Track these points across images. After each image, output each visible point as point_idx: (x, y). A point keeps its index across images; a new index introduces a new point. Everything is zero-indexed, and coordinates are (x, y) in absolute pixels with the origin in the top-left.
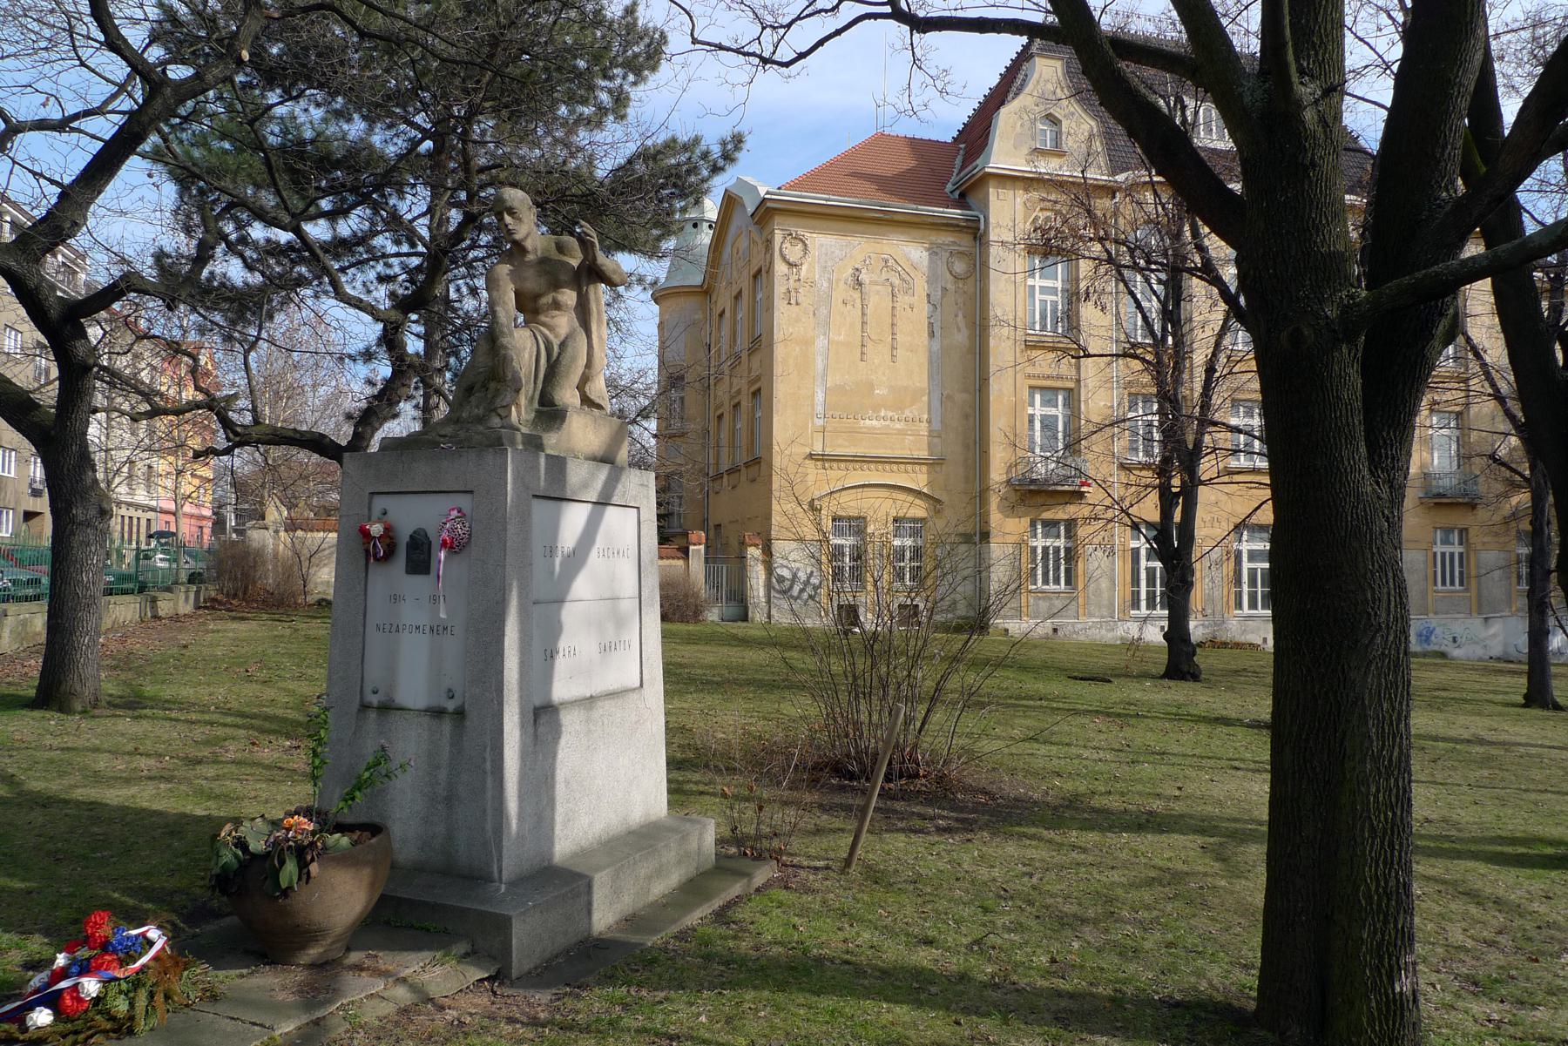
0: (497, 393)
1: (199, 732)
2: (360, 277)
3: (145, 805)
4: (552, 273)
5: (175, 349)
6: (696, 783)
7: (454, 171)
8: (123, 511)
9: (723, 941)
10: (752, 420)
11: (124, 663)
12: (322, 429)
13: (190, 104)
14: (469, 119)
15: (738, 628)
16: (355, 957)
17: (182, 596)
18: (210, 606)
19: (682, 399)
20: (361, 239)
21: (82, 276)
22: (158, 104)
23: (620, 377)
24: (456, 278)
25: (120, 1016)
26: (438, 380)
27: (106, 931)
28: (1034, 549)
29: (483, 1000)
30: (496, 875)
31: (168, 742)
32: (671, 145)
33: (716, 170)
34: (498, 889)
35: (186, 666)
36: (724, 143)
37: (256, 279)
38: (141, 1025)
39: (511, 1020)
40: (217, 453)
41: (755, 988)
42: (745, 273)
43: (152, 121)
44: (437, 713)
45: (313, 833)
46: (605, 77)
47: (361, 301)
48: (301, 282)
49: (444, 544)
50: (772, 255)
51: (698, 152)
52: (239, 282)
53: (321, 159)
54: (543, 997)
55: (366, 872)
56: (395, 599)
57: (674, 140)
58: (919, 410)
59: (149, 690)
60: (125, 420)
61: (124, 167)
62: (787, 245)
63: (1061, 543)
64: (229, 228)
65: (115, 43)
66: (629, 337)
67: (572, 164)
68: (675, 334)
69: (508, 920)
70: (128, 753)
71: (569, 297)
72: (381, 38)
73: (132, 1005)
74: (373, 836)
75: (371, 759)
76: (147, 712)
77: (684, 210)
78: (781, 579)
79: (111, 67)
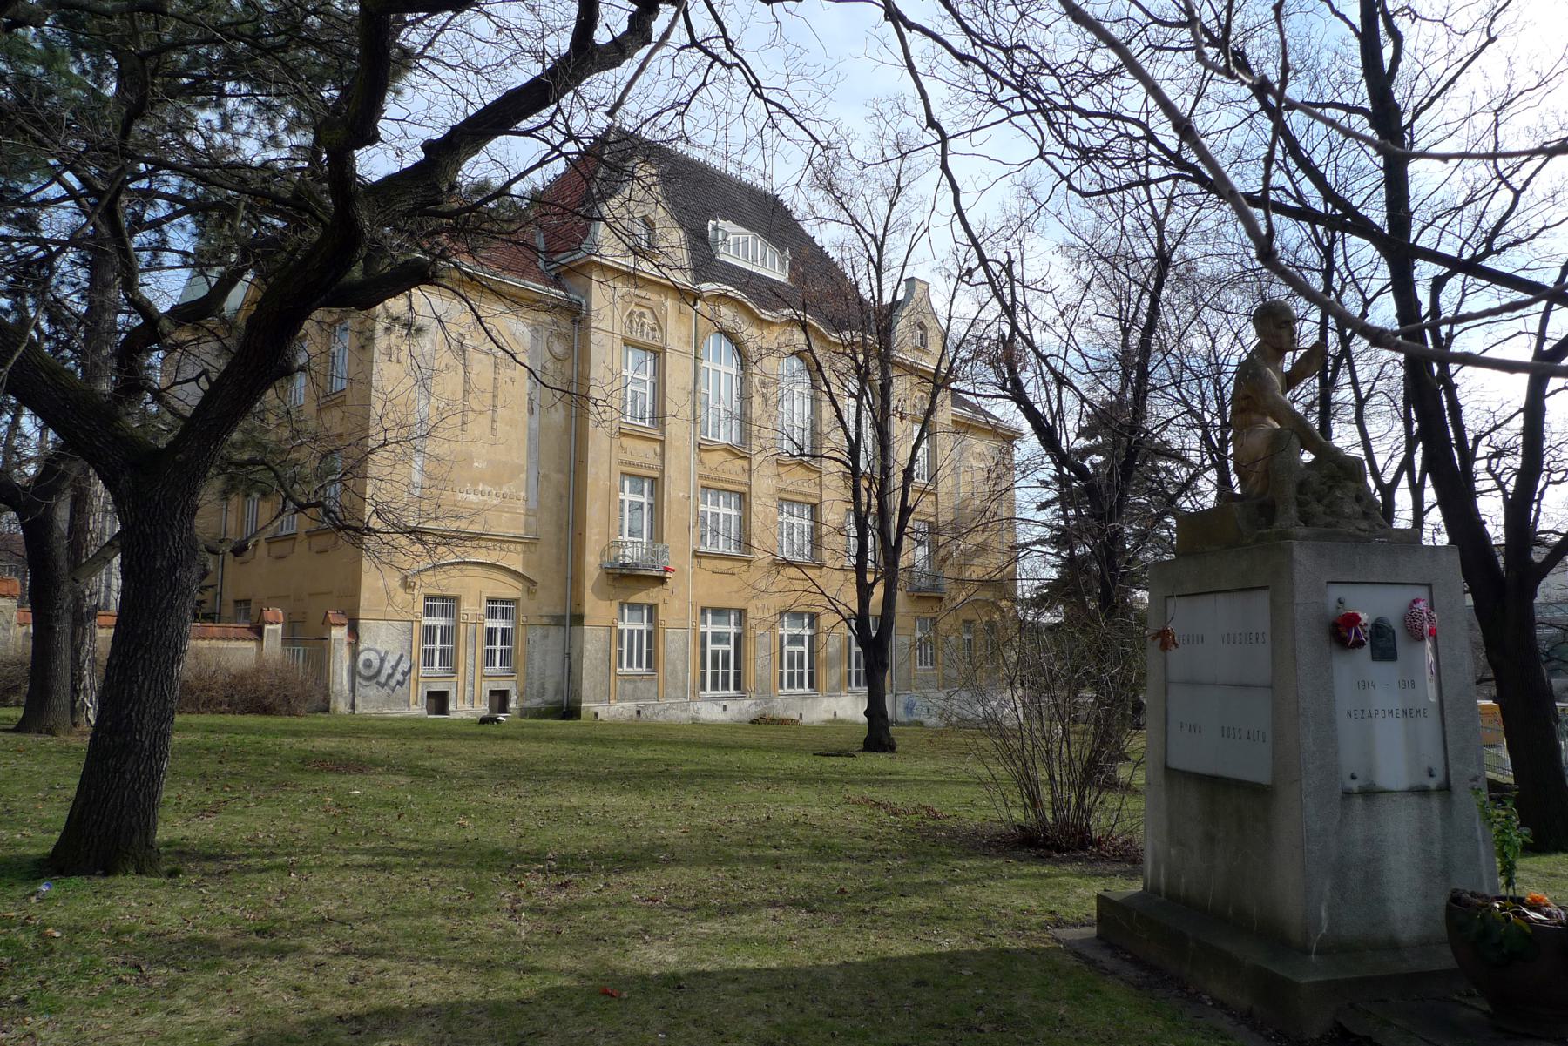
28: (622, 631)
56: (1364, 685)
58: (518, 486)
63: (645, 627)
78: (368, 664)
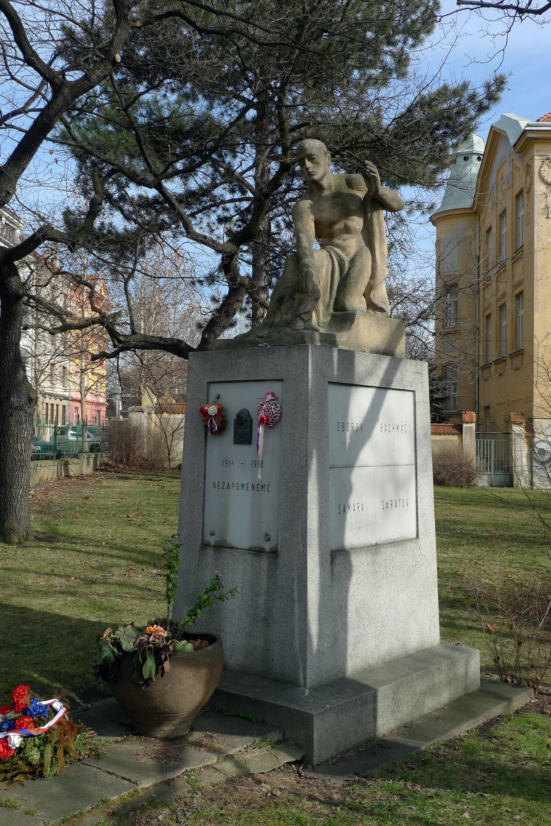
0: (301, 302)
1: (95, 561)
2: (206, 220)
3: (57, 611)
4: (344, 204)
5: (78, 281)
6: (466, 619)
7: (273, 132)
8: (47, 400)
9: (485, 751)
10: (516, 318)
11: (46, 509)
12: (181, 337)
13: (83, 97)
14: (281, 91)
15: (504, 493)
16: (196, 736)
17: (85, 461)
18: (103, 468)
19: (456, 303)
20: (205, 191)
21: (18, 232)
22: (60, 100)
23: (405, 287)
24: (276, 216)
25: (34, 763)
26: (263, 296)
27: (25, 700)
29: (291, 779)
30: (302, 681)
31: (74, 567)
32: (444, 93)
33: (482, 109)
34: (304, 693)
35: (87, 512)
36: (488, 86)
37: (132, 226)
38: (48, 771)
39: (311, 798)
40: (109, 356)
41: (512, 794)
42: (509, 195)
43: (56, 114)
44: (257, 552)
45: (167, 639)
46: (390, 43)
47: (205, 237)
48: (163, 226)
49: (262, 421)
50: (532, 177)
51: (466, 95)
52: (120, 229)
53: (176, 132)
54: (337, 782)
55: (204, 672)
56: (226, 463)
57: (445, 88)
59: (62, 528)
60: (46, 334)
61: (39, 149)
62: (545, 168)
64: (113, 189)
65: (31, 59)
66: (410, 250)
67: (363, 117)
68: (449, 249)
69: (311, 717)
70: (47, 574)
71: (357, 223)
72: (217, 33)
73: (42, 756)
74: (210, 644)
75: (209, 585)
76: (60, 544)
77: (455, 146)
79: (31, 78)
